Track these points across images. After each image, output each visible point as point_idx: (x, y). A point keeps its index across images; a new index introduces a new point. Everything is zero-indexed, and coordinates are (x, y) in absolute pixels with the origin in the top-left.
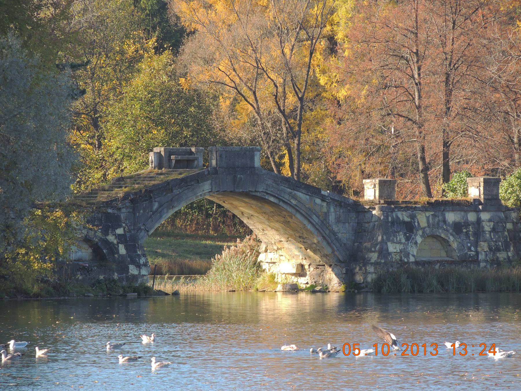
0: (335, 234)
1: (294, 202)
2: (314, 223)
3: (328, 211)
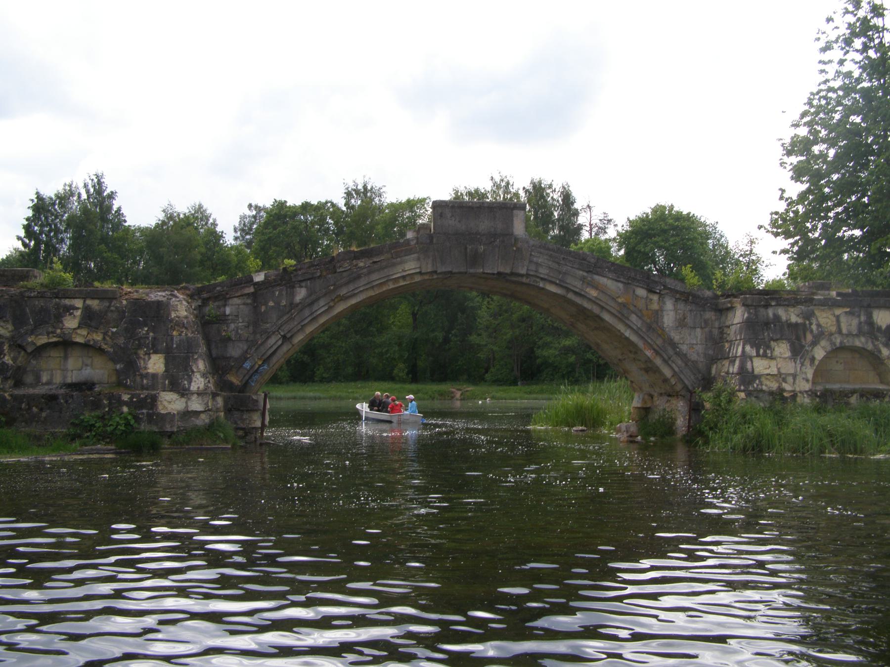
0: (674, 345)
1: (593, 293)
2: (635, 328)
3: (661, 310)
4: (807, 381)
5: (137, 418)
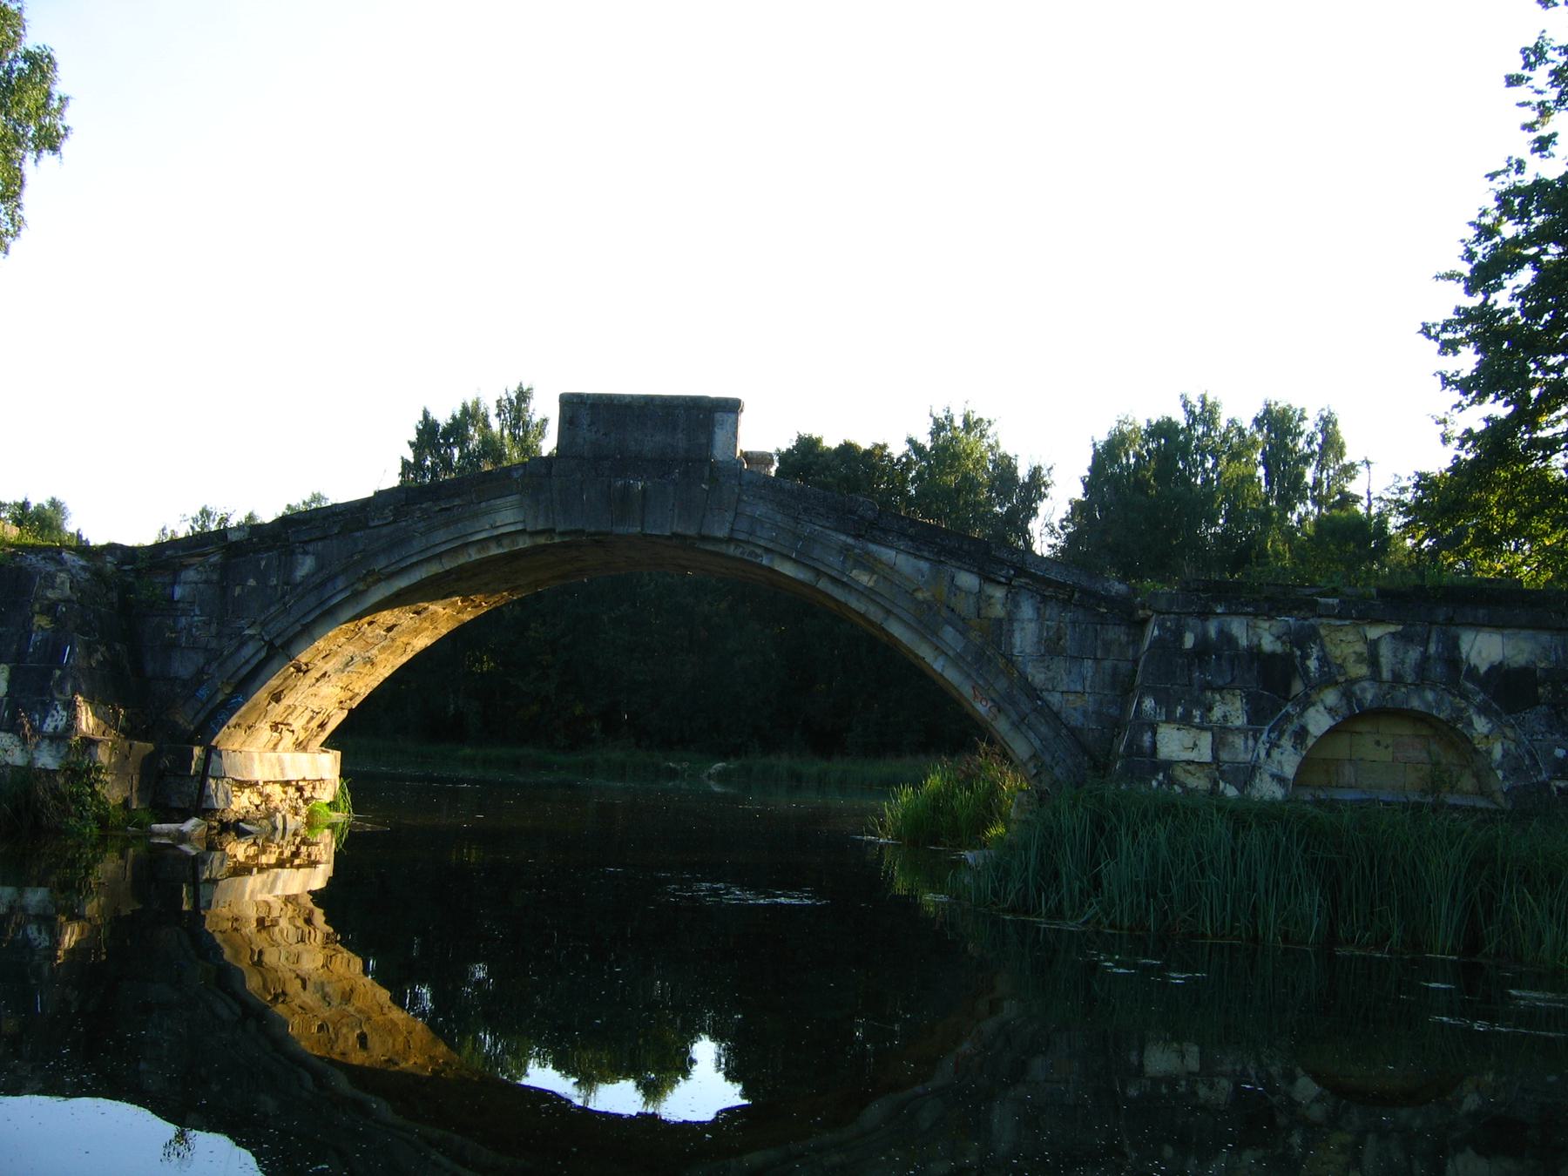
0: (1033, 692)
1: (865, 579)
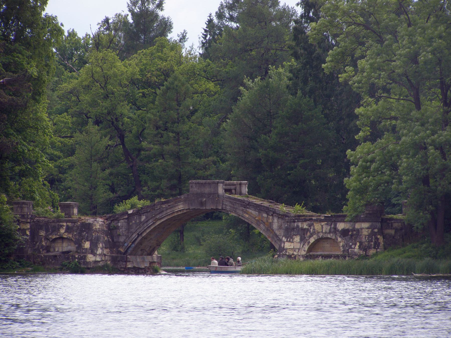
1: (247, 216)
3: (273, 222)
4: (305, 251)
5: (80, 263)
